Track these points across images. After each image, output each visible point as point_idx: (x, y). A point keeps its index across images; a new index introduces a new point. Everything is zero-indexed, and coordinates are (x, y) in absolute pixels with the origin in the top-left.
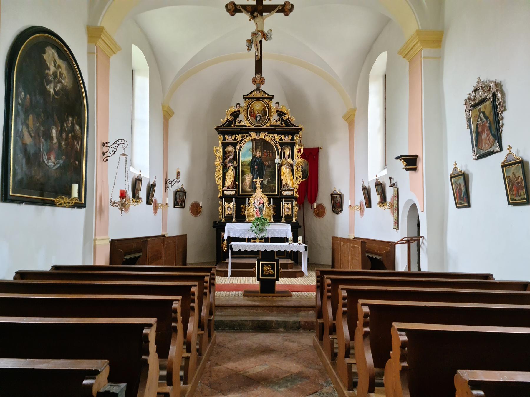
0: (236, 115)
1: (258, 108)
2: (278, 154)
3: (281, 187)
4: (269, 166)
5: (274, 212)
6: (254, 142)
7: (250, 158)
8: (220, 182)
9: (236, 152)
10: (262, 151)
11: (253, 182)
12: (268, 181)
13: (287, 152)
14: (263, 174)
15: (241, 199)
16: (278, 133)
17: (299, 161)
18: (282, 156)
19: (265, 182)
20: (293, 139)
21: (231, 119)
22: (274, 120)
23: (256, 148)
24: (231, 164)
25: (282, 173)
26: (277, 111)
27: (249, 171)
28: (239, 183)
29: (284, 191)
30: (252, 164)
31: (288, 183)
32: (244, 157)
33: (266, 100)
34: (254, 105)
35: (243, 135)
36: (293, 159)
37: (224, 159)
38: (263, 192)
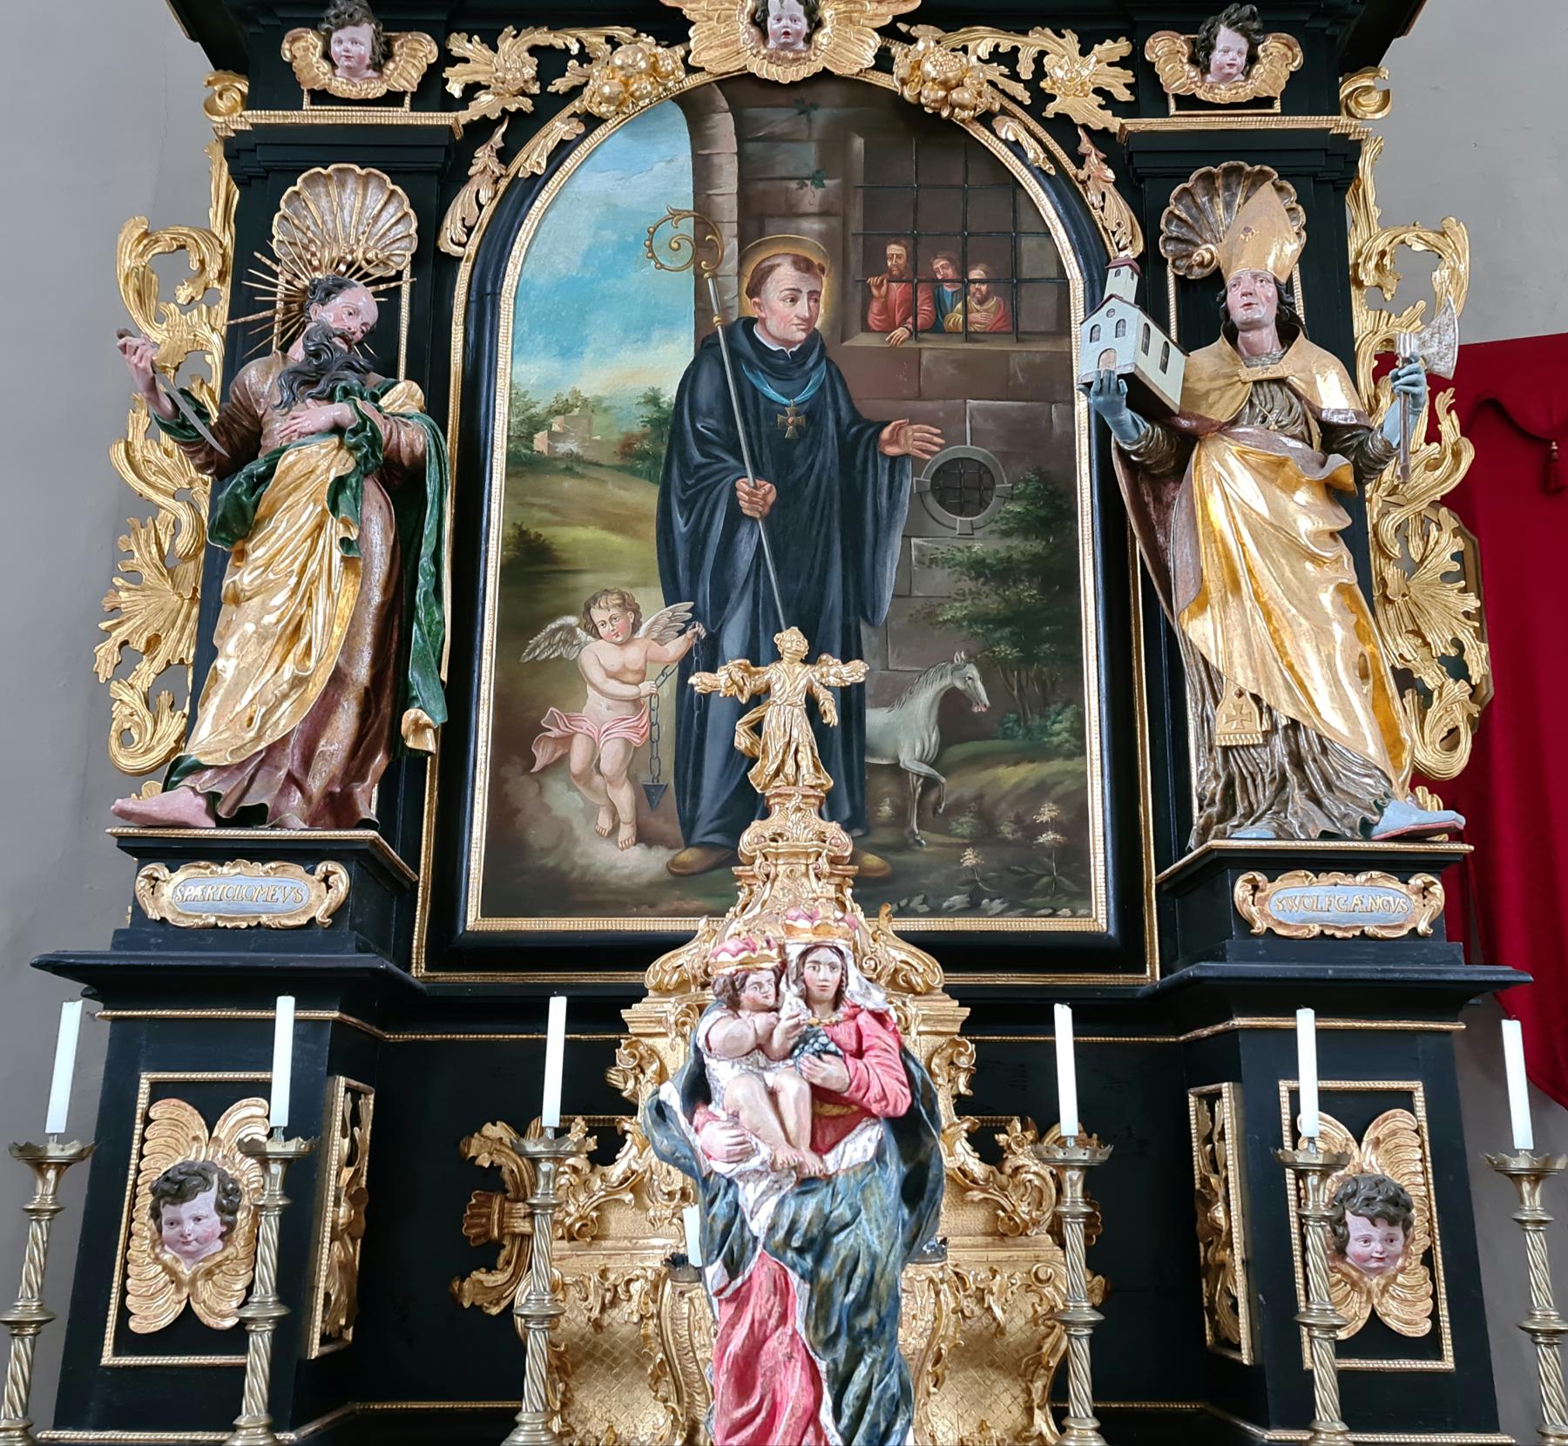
4: (959, 487)
6: (724, 125)
7: (666, 363)
10: (851, 263)
11: (693, 713)
12: (952, 708)
13: (1259, 243)
14: (861, 602)
19: (905, 731)
23: (760, 215)
24: (318, 414)
27: (645, 549)
28: (456, 734)
29: (1275, 863)
30: (681, 449)
31: (1332, 719)
32: (568, 352)
35: (567, 40)
38: (871, 892)
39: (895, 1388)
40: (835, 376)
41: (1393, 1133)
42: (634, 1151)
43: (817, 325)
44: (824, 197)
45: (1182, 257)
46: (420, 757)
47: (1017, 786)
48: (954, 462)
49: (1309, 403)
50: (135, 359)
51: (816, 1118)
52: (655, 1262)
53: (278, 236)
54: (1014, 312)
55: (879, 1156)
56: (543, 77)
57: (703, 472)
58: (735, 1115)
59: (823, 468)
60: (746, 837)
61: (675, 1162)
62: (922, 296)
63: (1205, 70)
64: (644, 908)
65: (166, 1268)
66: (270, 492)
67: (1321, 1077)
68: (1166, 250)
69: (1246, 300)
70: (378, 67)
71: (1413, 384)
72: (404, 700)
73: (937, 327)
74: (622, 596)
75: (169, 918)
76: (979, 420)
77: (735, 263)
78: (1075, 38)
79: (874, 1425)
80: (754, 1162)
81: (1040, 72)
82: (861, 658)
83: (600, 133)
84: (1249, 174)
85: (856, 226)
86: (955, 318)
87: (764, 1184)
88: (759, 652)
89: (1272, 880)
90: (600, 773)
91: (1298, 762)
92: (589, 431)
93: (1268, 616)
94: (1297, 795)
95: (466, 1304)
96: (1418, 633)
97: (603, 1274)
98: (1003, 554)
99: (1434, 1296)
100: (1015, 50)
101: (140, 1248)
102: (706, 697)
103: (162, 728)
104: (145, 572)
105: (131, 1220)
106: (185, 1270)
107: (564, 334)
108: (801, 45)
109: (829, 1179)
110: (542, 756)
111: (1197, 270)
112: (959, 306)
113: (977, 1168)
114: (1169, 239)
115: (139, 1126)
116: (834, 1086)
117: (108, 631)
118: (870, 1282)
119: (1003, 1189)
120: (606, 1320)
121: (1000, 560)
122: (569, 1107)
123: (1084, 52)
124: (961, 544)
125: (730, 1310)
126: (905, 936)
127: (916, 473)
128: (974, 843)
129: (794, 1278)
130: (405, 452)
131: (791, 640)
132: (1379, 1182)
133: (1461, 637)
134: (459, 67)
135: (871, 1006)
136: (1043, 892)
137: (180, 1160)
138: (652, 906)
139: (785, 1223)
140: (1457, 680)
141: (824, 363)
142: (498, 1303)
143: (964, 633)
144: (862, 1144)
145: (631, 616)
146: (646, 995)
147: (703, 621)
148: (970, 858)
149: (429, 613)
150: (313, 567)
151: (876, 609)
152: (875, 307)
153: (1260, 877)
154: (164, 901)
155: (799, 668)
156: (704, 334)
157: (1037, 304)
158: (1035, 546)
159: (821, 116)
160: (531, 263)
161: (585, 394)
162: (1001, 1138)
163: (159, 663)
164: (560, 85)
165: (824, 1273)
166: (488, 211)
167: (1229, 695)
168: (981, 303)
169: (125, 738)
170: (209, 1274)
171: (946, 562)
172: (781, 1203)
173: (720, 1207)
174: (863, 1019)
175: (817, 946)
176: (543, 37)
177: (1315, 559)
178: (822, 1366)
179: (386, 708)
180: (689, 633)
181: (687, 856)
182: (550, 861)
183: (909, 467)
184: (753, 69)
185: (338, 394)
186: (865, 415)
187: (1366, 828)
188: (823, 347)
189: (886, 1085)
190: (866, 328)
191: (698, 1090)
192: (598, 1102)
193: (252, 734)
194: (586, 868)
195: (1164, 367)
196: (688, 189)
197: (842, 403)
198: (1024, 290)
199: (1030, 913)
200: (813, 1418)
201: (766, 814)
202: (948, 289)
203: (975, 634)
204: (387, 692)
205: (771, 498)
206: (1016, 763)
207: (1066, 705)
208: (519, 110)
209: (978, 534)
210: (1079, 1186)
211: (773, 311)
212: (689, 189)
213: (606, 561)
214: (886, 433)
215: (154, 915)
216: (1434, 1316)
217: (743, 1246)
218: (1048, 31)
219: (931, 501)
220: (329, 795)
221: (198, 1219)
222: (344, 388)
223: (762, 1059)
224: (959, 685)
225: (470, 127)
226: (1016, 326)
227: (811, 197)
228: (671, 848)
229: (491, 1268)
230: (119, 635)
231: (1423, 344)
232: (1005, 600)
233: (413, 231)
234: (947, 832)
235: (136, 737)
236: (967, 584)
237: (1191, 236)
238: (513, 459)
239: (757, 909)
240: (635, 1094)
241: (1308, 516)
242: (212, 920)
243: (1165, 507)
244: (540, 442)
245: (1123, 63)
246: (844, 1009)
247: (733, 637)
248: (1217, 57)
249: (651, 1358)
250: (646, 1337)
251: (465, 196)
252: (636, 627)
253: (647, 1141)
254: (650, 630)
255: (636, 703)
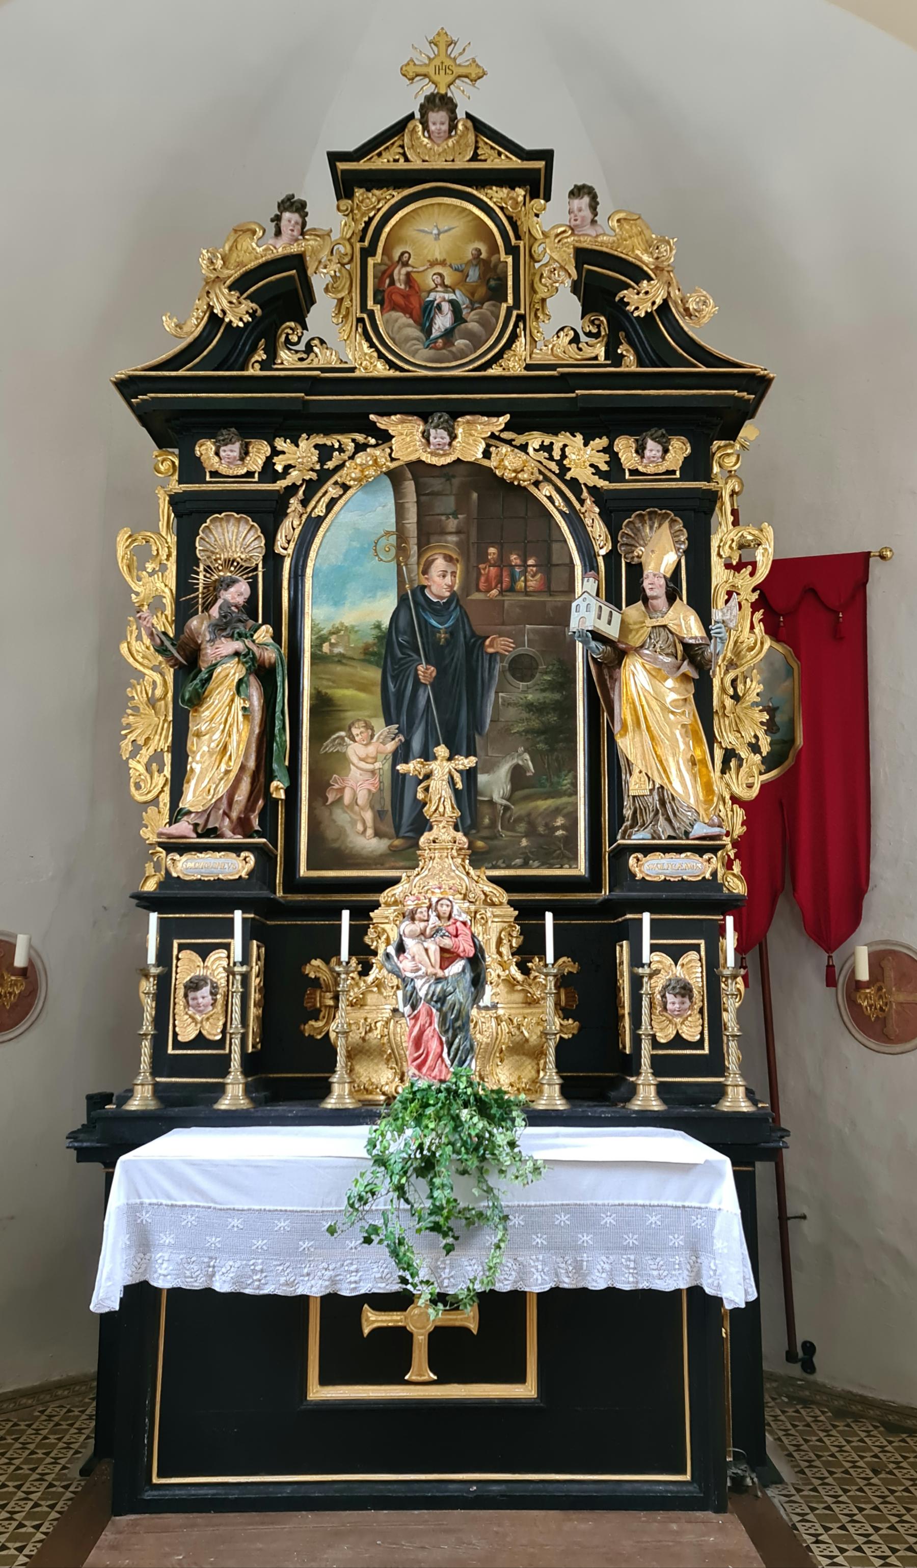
0: (281, 293)
1: (437, 250)
2: (590, 564)
3: (617, 818)
4: (521, 668)
5: (565, 1012)
6: (410, 487)
7: (382, 608)
8: (152, 785)
9: (272, 560)
10: (471, 556)
11: (399, 782)
12: (517, 773)
13: (661, 553)
14: (476, 723)
15: (301, 917)
16: (594, 422)
17: (740, 629)
18: (624, 584)
19: (495, 784)
20: (698, 465)
21: (239, 312)
22: (557, 333)
23: (428, 534)
24: (229, 646)
25: (623, 711)
26: (583, 256)
27: (375, 699)
28: (293, 791)
29: (646, 850)
30: (392, 650)
31: (677, 787)
33: (495, 196)
34: (410, 231)
35: (332, 441)
36: (701, 603)
37: (184, 610)
38: (477, 858)
39: (468, 1046)
40: (464, 615)
41: (690, 961)
42: (377, 970)
43: (455, 589)
44: (459, 523)
45: (629, 553)
46: (276, 801)
47: (545, 809)
48: (520, 656)
49: (677, 636)
50: (145, 623)
51: (442, 958)
52: (387, 1014)
53: (199, 548)
54: (548, 580)
55: (463, 970)
56: (322, 460)
57: (403, 662)
58: (413, 957)
59: (458, 659)
60: (422, 840)
61: (393, 973)
62: (505, 574)
63: (643, 457)
64: (379, 866)
65: (190, 1017)
66: (212, 685)
67: (652, 938)
68: (621, 550)
69: (650, 586)
70: (242, 459)
71: (719, 633)
72: (270, 777)
73: (511, 589)
74: (366, 722)
75: (181, 876)
76: (532, 636)
77: (415, 558)
78: (581, 437)
79: (461, 1057)
80: (420, 973)
81: (564, 456)
82: (475, 756)
83: (350, 493)
84: (660, 514)
85: (473, 538)
86: (521, 584)
87: (424, 980)
88: (427, 755)
89: (645, 856)
90: (357, 805)
91: (663, 802)
92: (349, 642)
93: (653, 738)
94: (661, 818)
95: (307, 1035)
96: (739, 732)
97: (366, 1019)
98: (542, 701)
99: (703, 1026)
100: (552, 444)
101: (180, 1008)
102: (404, 775)
103: (154, 781)
104: (141, 707)
105: (175, 998)
106: (198, 1017)
107: (335, 590)
108: (447, 447)
109: (446, 978)
110: (331, 797)
111: (636, 559)
112: (523, 578)
113: (519, 976)
114: (622, 545)
115: (174, 961)
116: (447, 947)
117: (126, 735)
118: (459, 1011)
119: (530, 985)
120: (367, 1038)
121: (540, 703)
122: (351, 953)
123: (586, 444)
124: (522, 696)
125: (413, 1021)
126: (492, 880)
127: (502, 661)
128: (526, 835)
129: (434, 1011)
130: (267, 662)
131: (442, 751)
132: (678, 981)
133: (758, 734)
134: (281, 456)
135: (461, 919)
136: (557, 858)
137: (192, 974)
138: (382, 865)
139: (431, 993)
140: (755, 754)
141: (458, 608)
142: (320, 1034)
143: (523, 738)
144: (457, 967)
145: (370, 732)
146: (380, 906)
147: (403, 734)
148: (524, 842)
149: (280, 737)
150: (230, 720)
151: (482, 726)
152: (483, 579)
153: (640, 856)
154: (178, 869)
155: (445, 763)
156: (401, 594)
157: (559, 574)
158: (557, 696)
159: (456, 481)
160: (319, 560)
161: (346, 624)
162: (530, 965)
163: (151, 751)
164: (330, 465)
165: (444, 1009)
166: (297, 532)
167: (636, 772)
168: (533, 576)
169: (138, 787)
170: (208, 1019)
171: (515, 705)
172: (430, 986)
173: (409, 988)
174: (458, 924)
175: (442, 899)
176: (320, 440)
177: (673, 713)
178: (444, 1039)
179: (262, 779)
180: (397, 739)
181: (397, 842)
182: (336, 845)
183: (498, 658)
184: (424, 459)
185: (236, 635)
186: (477, 633)
187: (687, 834)
188: (458, 600)
189: (465, 946)
190: (478, 590)
191: (401, 948)
192: (363, 952)
193: (210, 797)
194: (352, 848)
195: (609, 623)
196: (393, 520)
197: (467, 627)
198: (555, 570)
199: (551, 867)
200: (441, 1056)
201: (431, 829)
202: (517, 570)
203: (528, 739)
204: (262, 774)
205: (434, 674)
206: (546, 799)
207: (569, 772)
208: (311, 479)
209: (530, 691)
210: (553, 983)
211: (434, 582)
212: (394, 520)
213: (357, 705)
214: (487, 642)
215: (175, 875)
216: (702, 1033)
217: (417, 1001)
218: (568, 434)
219: (508, 675)
220: (239, 819)
221: (203, 998)
222: (238, 633)
223: (423, 938)
224: (520, 763)
225: (287, 488)
226: (549, 587)
227: (452, 524)
228: (390, 839)
229: (317, 1019)
230: (131, 737)
231: (724, 614)
232: (543, 723)
233: (263, 545)
234: (513, 830)
235: (143, 786)
236: (525, 715)
237: (633, 542)
238: (313, 656)
239: (427, 872)
240: (377, 947)
241: (672, 691)
242: (199, 877)
243: (614, 680)
244: (326, 648)
245: (604, 450)
246: (452, 921)
247: (416, 745)
248: (647, 453)
249: (386, 1052)
250: (384, 1044)
251: (287, 523)
252: (372, 736)
253: (383, 966)
254: (379, 738)
255: (373, 772)
